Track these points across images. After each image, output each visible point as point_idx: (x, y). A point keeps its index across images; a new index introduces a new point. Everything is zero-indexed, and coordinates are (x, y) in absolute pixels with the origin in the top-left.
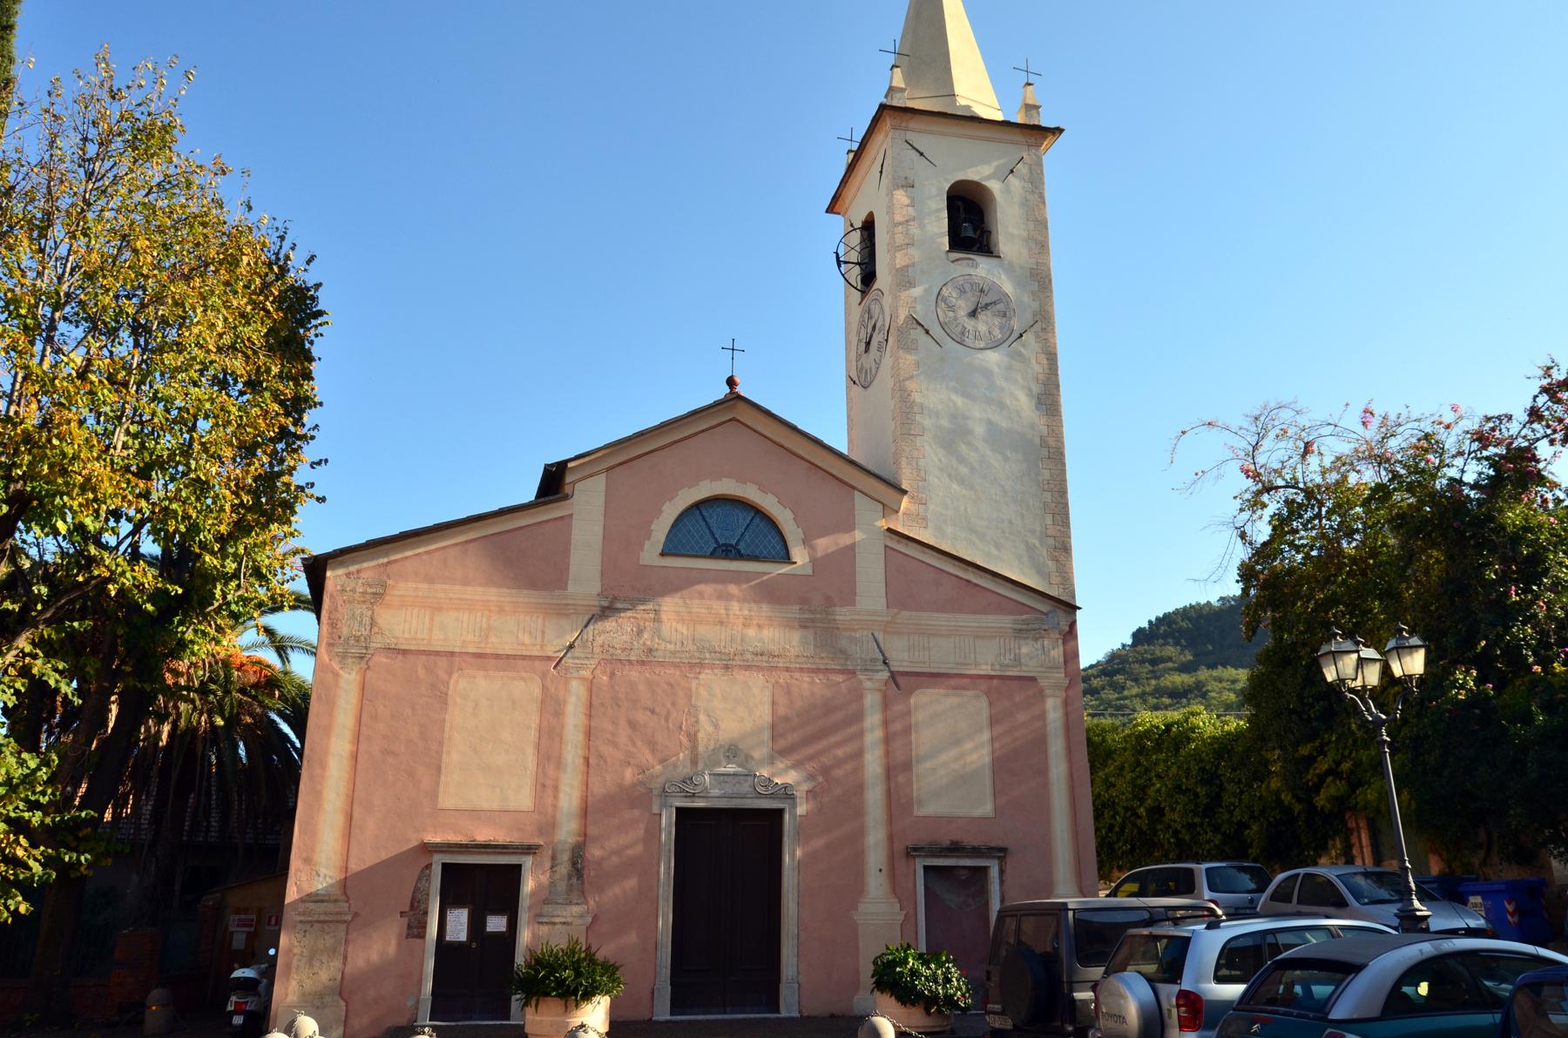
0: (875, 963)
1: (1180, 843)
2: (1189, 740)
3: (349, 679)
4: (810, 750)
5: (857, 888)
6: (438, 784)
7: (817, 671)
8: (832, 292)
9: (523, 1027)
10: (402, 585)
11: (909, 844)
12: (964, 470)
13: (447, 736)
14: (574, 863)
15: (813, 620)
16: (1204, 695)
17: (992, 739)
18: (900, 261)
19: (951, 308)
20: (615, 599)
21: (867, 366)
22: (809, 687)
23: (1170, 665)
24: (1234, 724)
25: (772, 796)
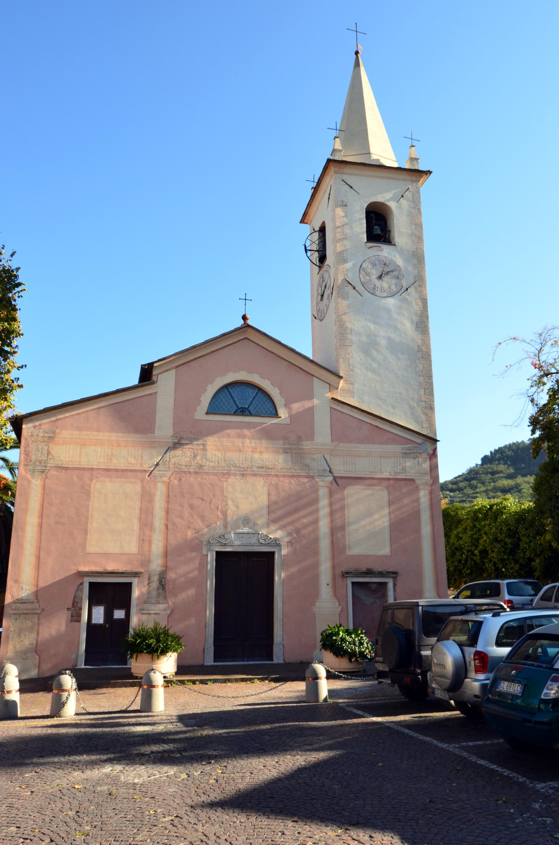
0: (322, 634)
1: (497, 569)
2: (502, 513)
3: (36, 483)
4: (289, 519)
5: (315, 595)
6: (85, 539)
7: (293, 476)
8: (304, 267)
9: (130, 668)
10: (64, 432)
11: (343, 570)
12: (374, 365)
13: (90, 513)
14: (161, 582)
15: (291, 449)
16: (520, 491)
17: (390, 513)
18: (339, 248)
19: (368, 274)
20: (181, 438)
21: (322, 308)
22: (289, 485)
23: (502, 475)
24: (528, 504)
25: (268, 545)
